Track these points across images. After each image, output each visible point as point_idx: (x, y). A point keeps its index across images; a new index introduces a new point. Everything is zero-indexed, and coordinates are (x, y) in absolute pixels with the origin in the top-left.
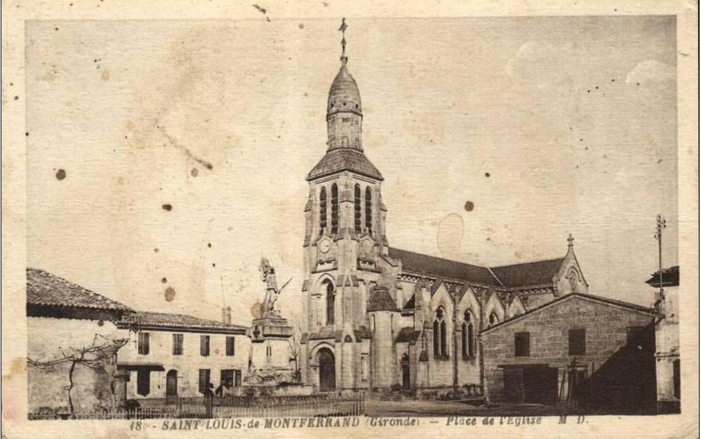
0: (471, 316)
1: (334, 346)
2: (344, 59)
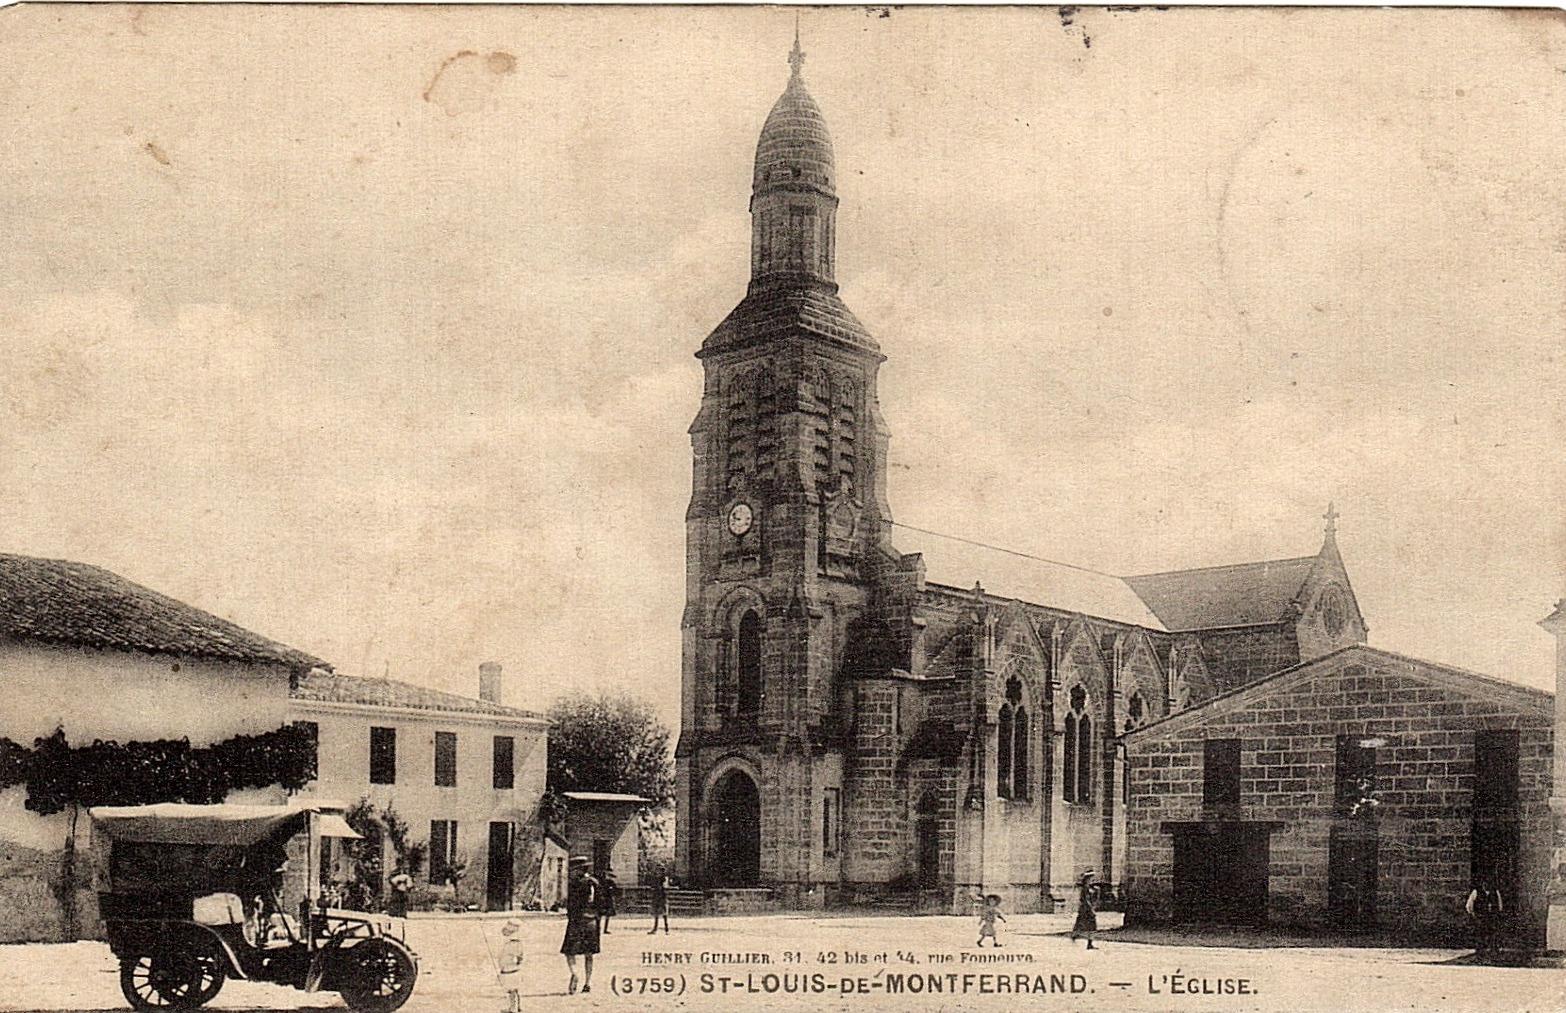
1: (758, 766)
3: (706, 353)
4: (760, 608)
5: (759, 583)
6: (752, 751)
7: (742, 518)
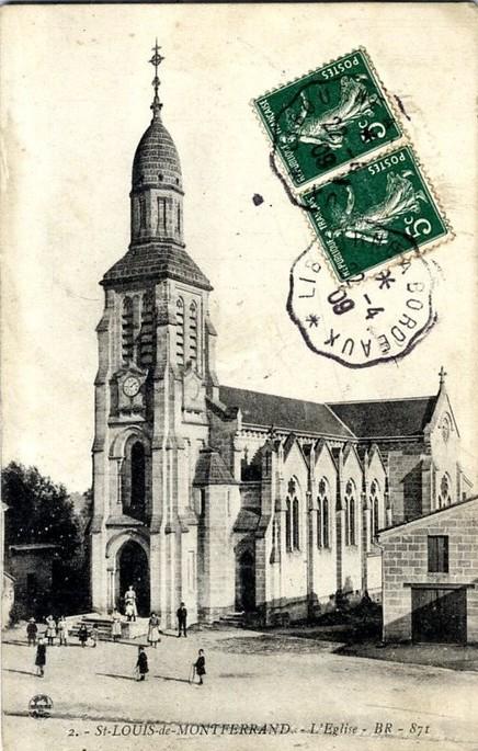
0: (296, 487)
2: (156, 106)
3: (108, 283)
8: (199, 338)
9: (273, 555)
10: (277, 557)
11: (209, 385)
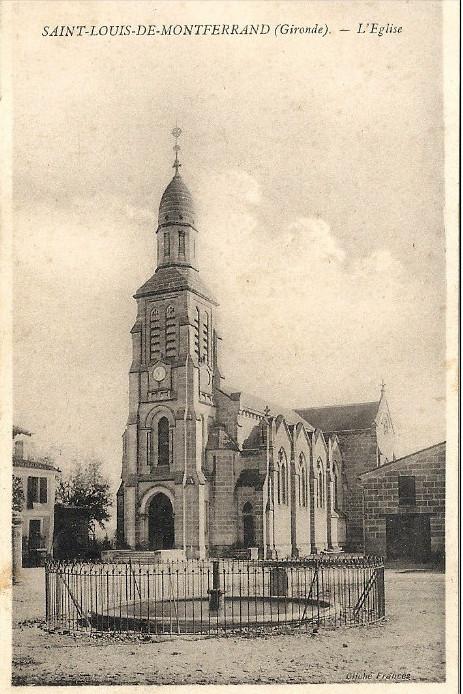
4: (170, 417)
5: (169, 404)
6: (171, 484)
7: (160, 373)
8: (210, 341)
9: (268, 505)
10: (271, 505)
11: (217, 377)
